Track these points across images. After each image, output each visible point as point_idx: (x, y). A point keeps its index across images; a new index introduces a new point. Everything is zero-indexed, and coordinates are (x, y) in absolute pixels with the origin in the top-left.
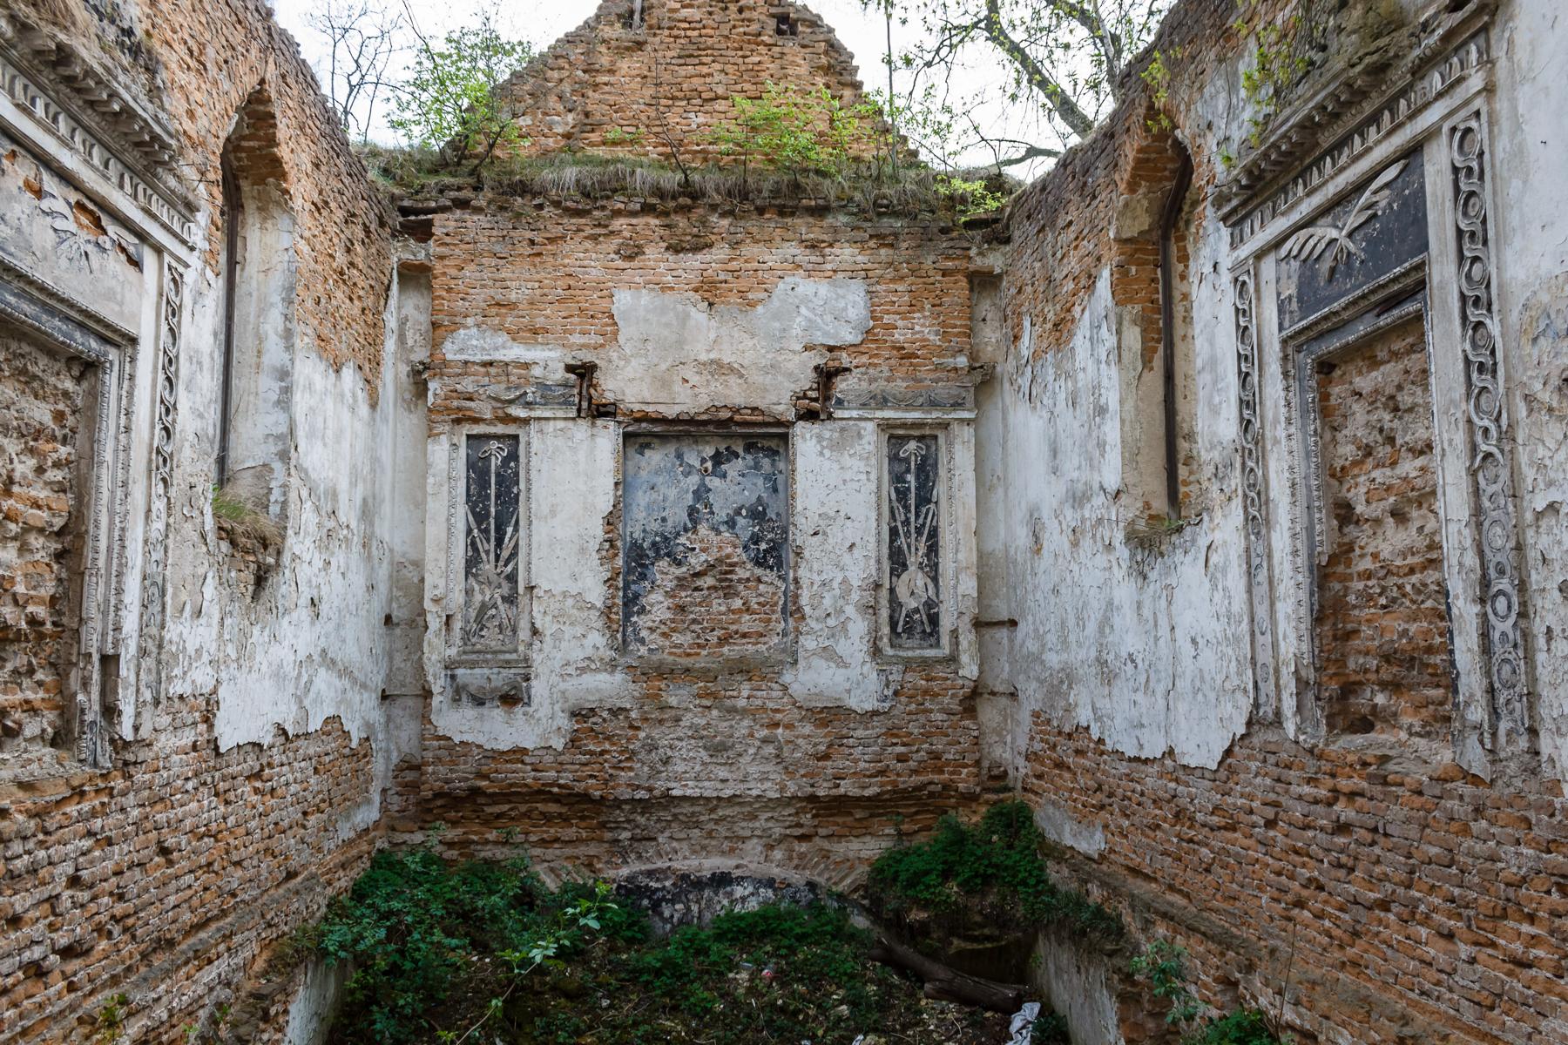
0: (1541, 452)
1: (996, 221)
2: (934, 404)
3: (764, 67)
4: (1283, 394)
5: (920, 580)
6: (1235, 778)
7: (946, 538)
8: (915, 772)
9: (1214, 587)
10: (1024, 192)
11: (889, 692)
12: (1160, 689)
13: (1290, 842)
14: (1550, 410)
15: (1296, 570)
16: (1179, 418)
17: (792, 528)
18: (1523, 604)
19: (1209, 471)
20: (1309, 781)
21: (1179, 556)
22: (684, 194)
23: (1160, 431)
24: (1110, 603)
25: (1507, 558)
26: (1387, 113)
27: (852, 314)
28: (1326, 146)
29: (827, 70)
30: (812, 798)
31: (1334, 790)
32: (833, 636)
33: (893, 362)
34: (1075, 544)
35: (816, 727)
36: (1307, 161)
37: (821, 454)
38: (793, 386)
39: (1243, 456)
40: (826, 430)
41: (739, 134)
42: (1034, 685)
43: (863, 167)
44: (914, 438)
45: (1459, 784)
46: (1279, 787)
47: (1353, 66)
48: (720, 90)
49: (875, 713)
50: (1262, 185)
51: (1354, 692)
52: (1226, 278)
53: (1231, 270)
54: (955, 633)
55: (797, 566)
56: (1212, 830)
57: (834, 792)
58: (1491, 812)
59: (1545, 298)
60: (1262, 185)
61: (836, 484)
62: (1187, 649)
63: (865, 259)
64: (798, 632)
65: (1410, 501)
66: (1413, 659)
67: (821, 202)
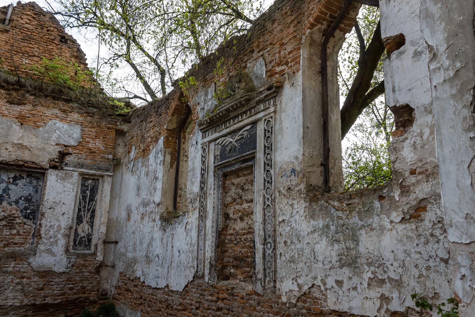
0: (282, 206)
1: (126, 115)
2: (99, 169)
3: (54, 50)
4: (213, 181)
5: (87, 227)
6: (188, 294)
7: (98, 213)
8: (75, 294)
9: (187, 235)
10: (137, 109)
11: (70, 265)
12: (166, 266)
13: (203, 314)
14: (285, 195)
15: (213, 232)
16: (179, 183)
17: (41, 206)
18: (275, 246)
19: (189, 200)
20: (210, 295)
21: (177, 225)
22: (17, 85)
23: (173, 186)
24: (152, 238)
25: (271, 233)
26: (249, 112)
27: (75, 136)
28: (232, 116)
29: (76, 57)
30: (34, 305)
31: (218, 298)
32: (52, 245)
33: (87, 153)
34: (142, 218)
35: (40, 278)
36: (226, 119)
37: (57, 181)
38: (49, 157)
39: (200, 197)
40: (60, 173)
41: (43, 70)
42: (122, 263)
43: (84, 90)
44: (91, 179)
45: (254, 296)
46: (201, 297)
47: (242, 98)
48: (36, 54)
49: (64, 273)
50: (213, 123)
51: (225, 268)
52: (199, 146)
53: (201, 144)
54: (96, 245)
55: (41, 219)
56: (178, 311)
57: (43, 302)
58: (262, 304)
59: (285, 166)
60: (213, 123)
61: (61, 192)
62: (177, 254)
63: (82, 119)
64: (38, 243)
65: (245, 215)
66: (242, 259)
67: (69, 98)
